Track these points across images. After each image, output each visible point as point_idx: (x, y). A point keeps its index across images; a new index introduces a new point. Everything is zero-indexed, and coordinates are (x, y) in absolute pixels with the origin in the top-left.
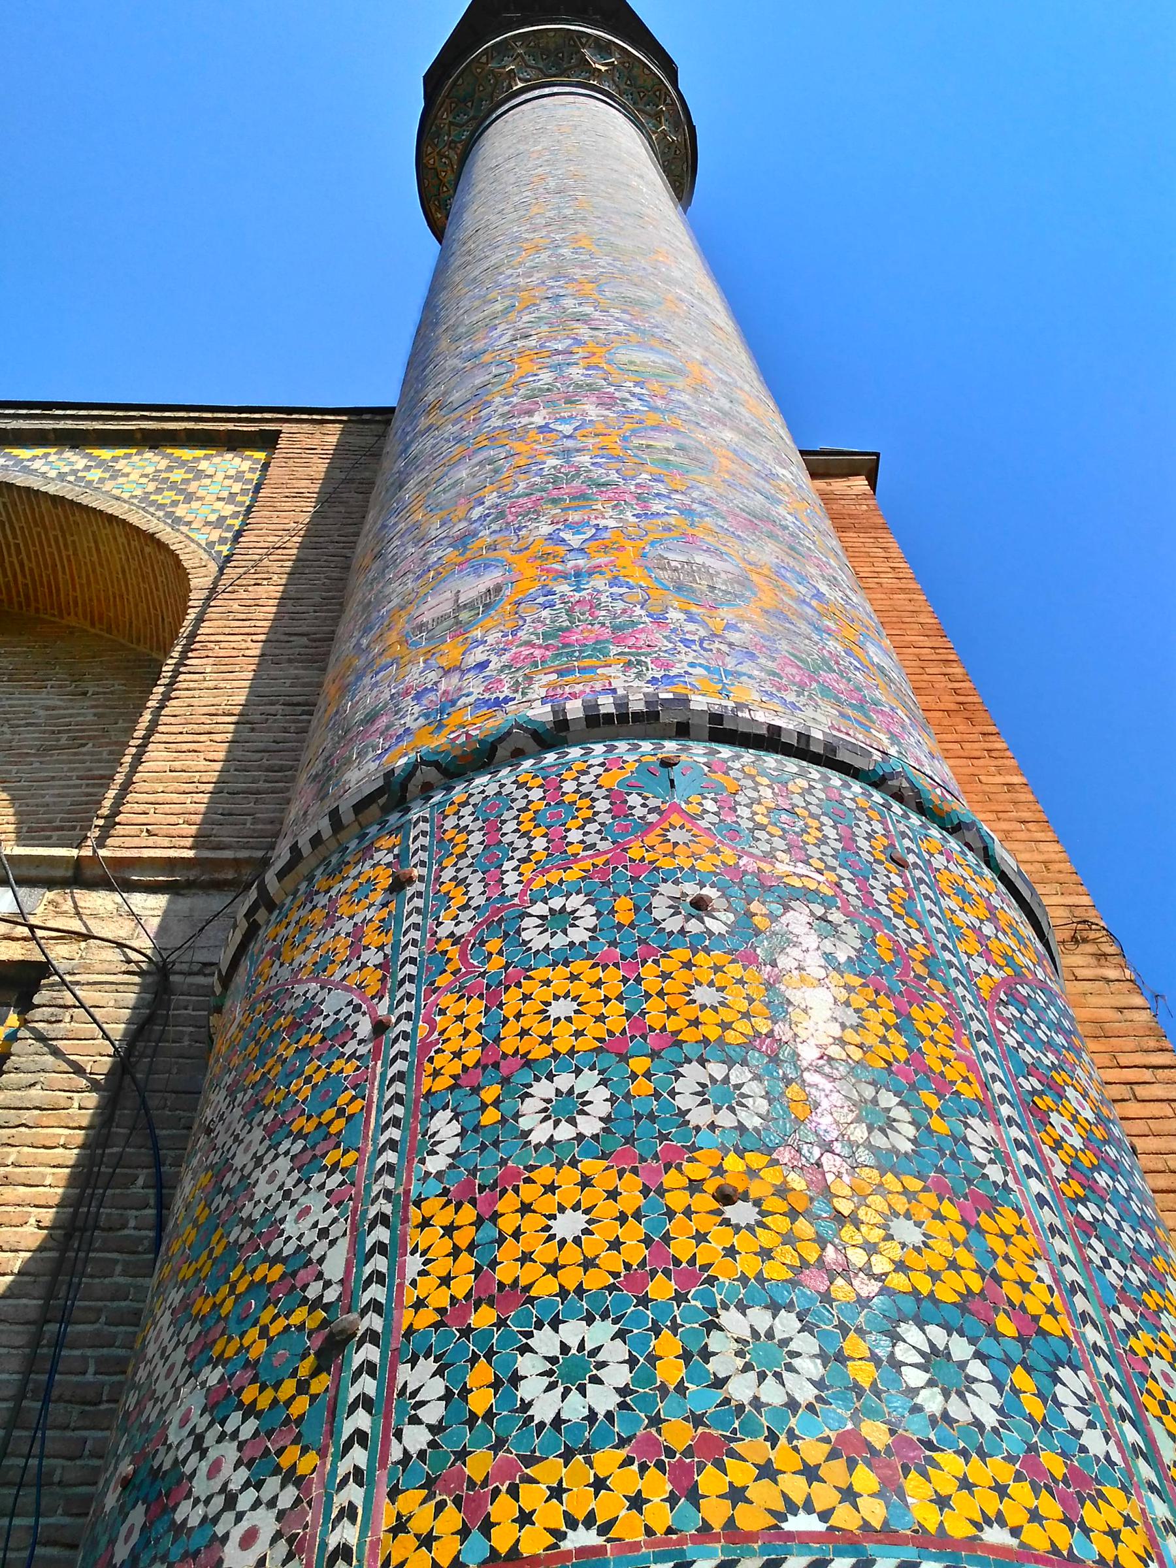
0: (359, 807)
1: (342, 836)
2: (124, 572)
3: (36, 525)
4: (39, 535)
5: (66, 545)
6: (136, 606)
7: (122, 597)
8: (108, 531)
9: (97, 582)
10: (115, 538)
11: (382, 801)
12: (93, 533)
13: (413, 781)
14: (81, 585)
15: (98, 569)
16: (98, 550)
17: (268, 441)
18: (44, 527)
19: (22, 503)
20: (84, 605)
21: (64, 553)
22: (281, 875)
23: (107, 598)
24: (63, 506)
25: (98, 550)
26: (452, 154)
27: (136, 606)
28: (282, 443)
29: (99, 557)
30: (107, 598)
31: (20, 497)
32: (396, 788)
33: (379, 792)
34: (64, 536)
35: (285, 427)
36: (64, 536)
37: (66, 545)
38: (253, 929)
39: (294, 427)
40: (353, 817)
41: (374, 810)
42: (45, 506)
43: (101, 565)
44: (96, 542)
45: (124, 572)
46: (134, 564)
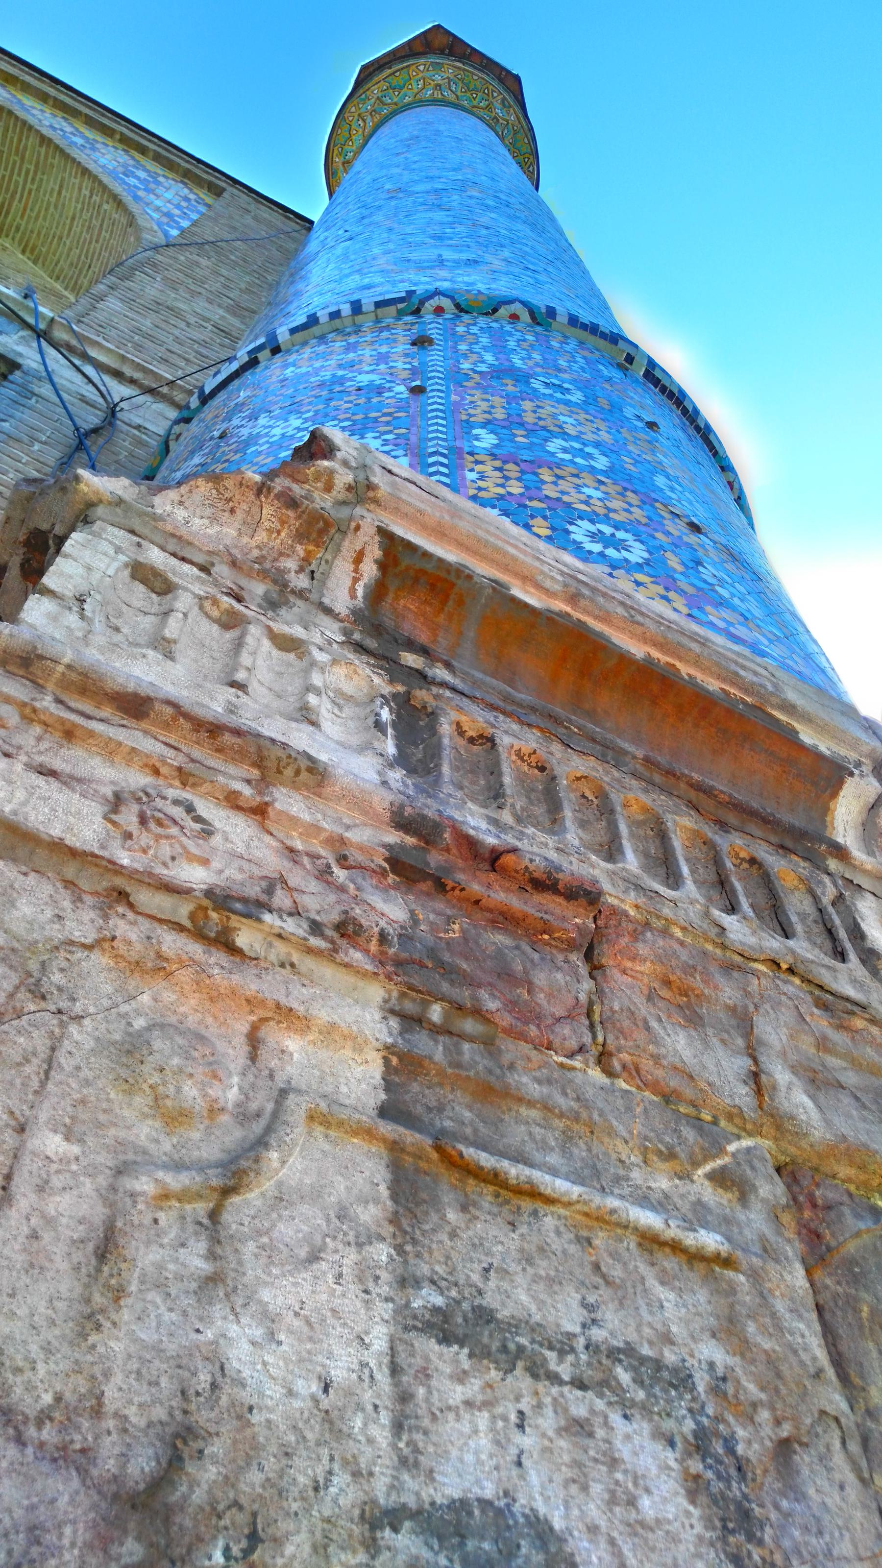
0: (378, 305)
1: (359, 319)
2: (73, 218)
3: (17, 153)
4: (15, 162)
5: (33, 180)
6: (70, 249)
7: (61, 238)
8: (77, 181)
9: (45, 219)
10: (80, 189)
11: (400, 306)
12: (63, 179)
13: (431, 302)
14: (30, 217)
15: (52, 209)
16: (60, 193)
17: (218, 192)
18: (23, 159)
19: (14, 132)
20: (24, 233)
21: (28, 185)
22: (293, 331)
23: (46, 236)
24: (48, 146)
25: (60, 193)
26: (368, 119)
27: (70, 249)
28: (225, 194)
29: (57, 200)
30: (46, 236)
31: (15, 125)
32: (415, 301)
33: (401, 300)
34: (35, 172)
35: (229, 189)
36: (35, 172)
37: (33, 180)
38: (253, 363)
39: (235, 191)
40: (372, 308)
41: (392, 310)
42: (33, 141)
43: (56, 207)
44: (61, 187)
45: (73, 218)
46: (86, 216)
